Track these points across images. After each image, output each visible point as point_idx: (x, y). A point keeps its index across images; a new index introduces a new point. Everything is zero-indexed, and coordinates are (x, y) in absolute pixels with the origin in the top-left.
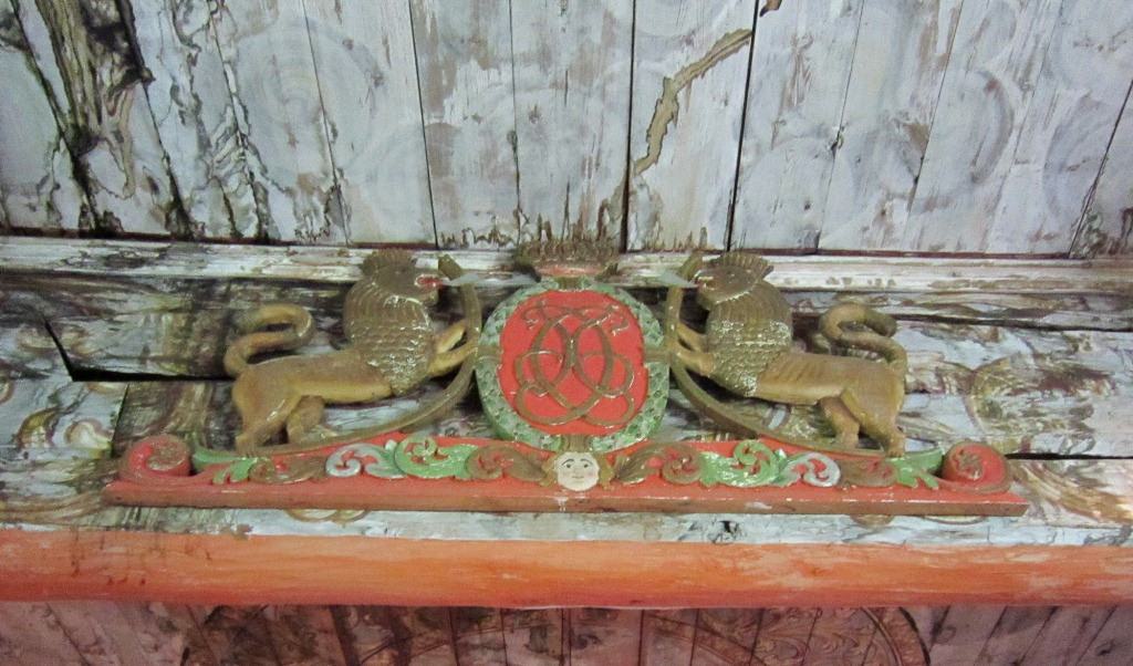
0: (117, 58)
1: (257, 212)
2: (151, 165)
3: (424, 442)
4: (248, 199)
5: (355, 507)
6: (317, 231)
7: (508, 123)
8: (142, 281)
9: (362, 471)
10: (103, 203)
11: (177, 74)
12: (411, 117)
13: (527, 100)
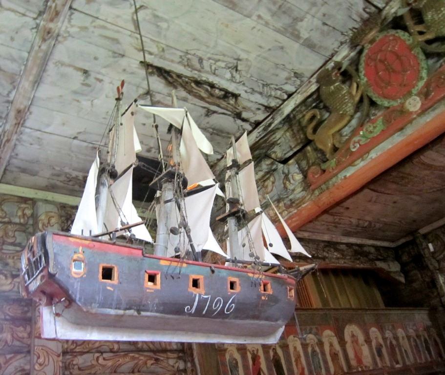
0: (231, 98)
1: (283, 92)
2: (254, 107)
3: (369, 127)
4: (279, 92)
5: (365, 154)
6: (299, 83)
7: (319, 23)
8: (275, 128)
9: (360, 145)
10: (252, 120)
11: (243, 89)
12: (296, 46)
13: (319, 15)
